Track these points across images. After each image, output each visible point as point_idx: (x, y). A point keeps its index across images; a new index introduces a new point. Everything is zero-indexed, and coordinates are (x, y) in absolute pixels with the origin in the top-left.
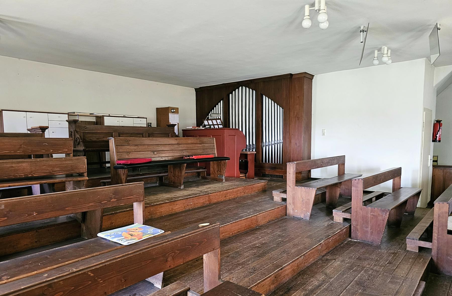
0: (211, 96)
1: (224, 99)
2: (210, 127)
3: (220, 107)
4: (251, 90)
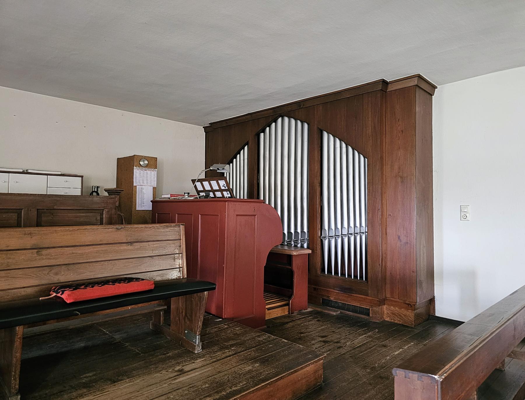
0: (232, 137)
1: (250, 143)
2: (207, 196)
3: (244, 155)
4: (299, 123)
